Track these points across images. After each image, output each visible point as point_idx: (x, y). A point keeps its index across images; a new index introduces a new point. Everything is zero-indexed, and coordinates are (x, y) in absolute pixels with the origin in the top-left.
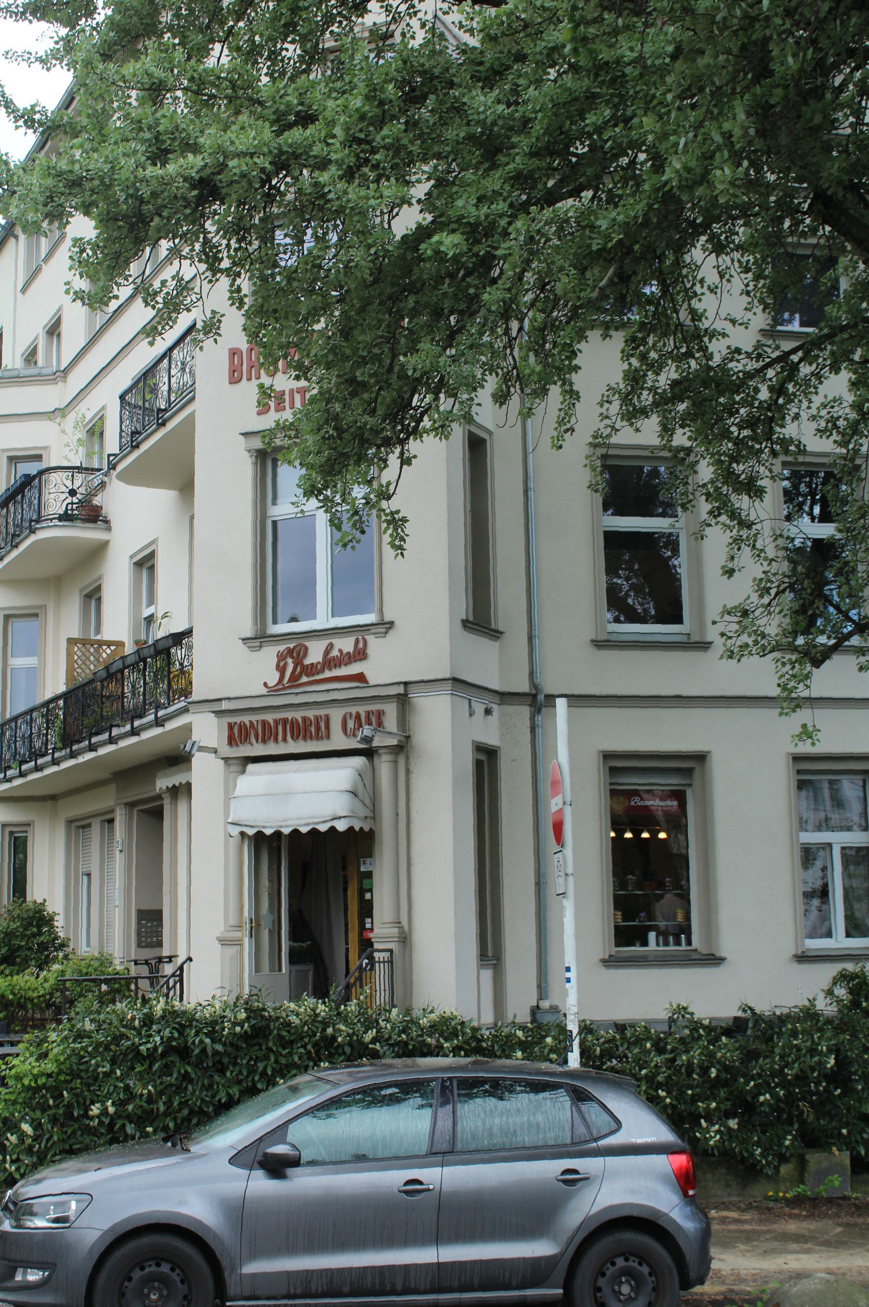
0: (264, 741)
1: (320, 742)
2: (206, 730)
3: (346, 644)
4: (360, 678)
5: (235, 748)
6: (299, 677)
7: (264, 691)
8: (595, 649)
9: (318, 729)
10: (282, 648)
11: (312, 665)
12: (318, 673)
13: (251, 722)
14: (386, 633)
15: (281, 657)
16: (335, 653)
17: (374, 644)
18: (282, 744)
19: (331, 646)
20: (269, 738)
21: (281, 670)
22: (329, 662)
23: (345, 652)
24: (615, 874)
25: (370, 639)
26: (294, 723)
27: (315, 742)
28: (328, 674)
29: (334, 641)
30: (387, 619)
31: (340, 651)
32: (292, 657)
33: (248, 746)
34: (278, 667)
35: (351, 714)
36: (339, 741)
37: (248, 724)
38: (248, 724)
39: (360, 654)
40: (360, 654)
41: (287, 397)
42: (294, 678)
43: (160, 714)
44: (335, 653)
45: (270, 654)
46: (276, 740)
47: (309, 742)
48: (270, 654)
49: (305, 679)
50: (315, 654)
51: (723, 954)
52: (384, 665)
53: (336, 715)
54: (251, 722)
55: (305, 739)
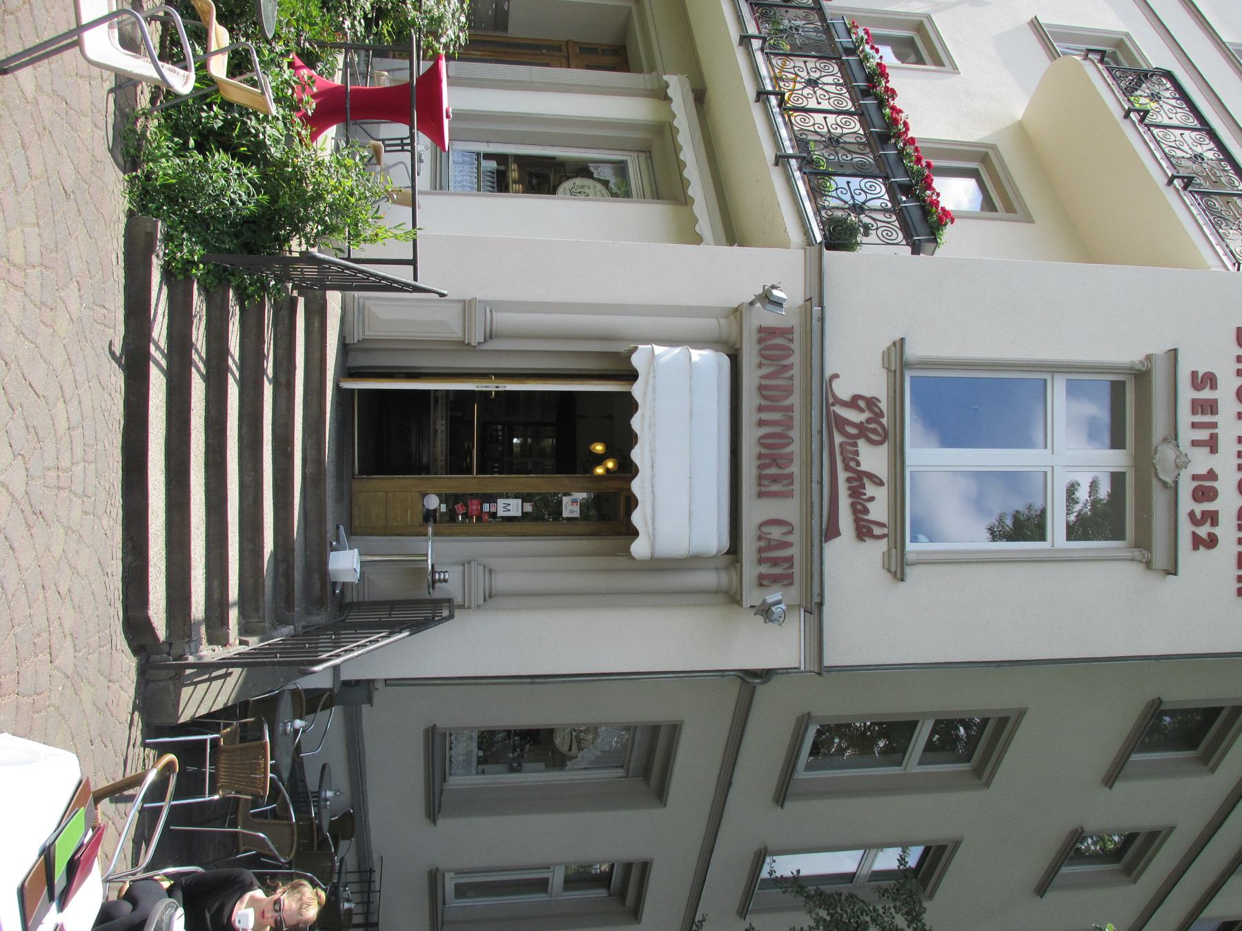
0: (761, 388)
1: (754, 481)
2: (771, 269)
3: (878, 511)
4: (832, 531)
5: (755, 336)
6: (843, 433)
7: (828, 373)
8: (798, 718)
9: (775, 479)
10: (883, 406)
11: (857, 453)
12: (844, 460)
13: (791, 367)
14: (889, 571)
15: (871, 403)
16: (870, 490)
17: (876, 549)
18: (756, 417)
19: (881, 483)
20: (764, 397)
21: (853, 403)
22: (859, 479)
23: (870, 505)
24: (528, 730)
25: (883, 545)
26: (785, 439)
27: (754, 472)
28: (842, 476)
29: (884, 490)
30: (908, 570)
31: (872, 499)
32: (869, 421)
33: (756, 360)
34: (856, 398)
35: (790, 533)
36: (754, 512)
37: (787, 362)
38: (787, 362)
39: (864, 531)
40: (864, 531)
41: (1207, 418)
42: (841, 423)
43: (793, 162)
44: (870, 490)
45: (875, 385)
46: (761, 409)
47: (755, 463)
48: (875, 385)
49: (838, 439)
50: (873, 459)
51: (440, 821)
52: (850, 564)
53: (789, 509)
54: (791, 367)
55: (760, 457)
